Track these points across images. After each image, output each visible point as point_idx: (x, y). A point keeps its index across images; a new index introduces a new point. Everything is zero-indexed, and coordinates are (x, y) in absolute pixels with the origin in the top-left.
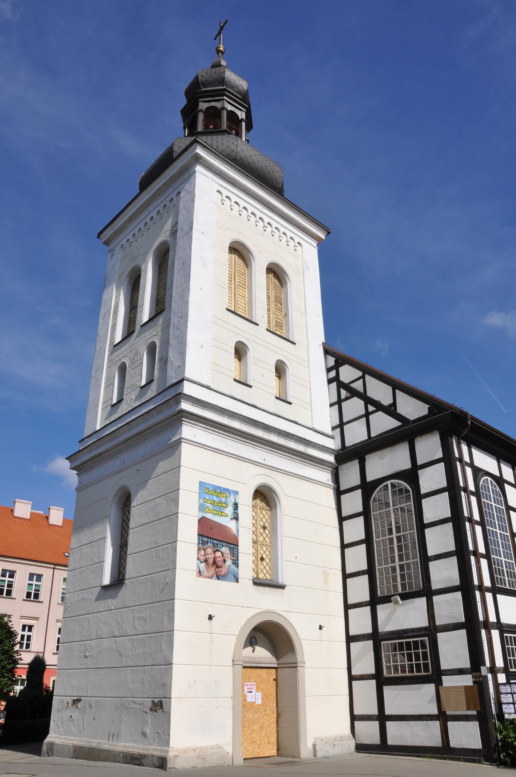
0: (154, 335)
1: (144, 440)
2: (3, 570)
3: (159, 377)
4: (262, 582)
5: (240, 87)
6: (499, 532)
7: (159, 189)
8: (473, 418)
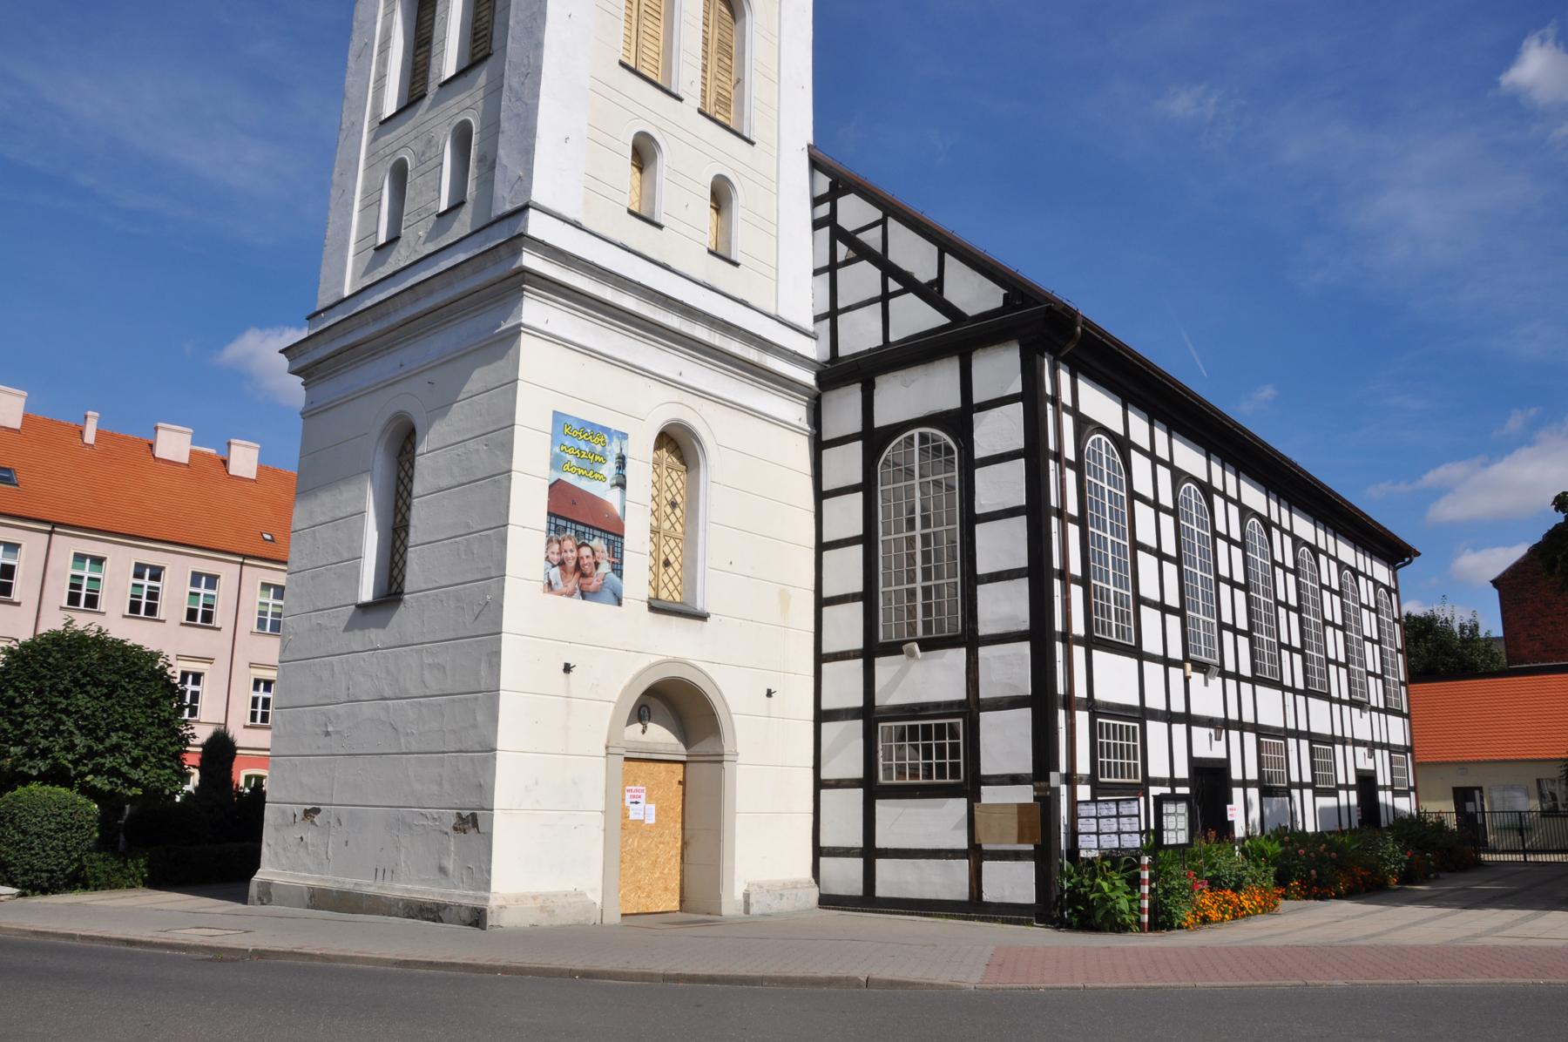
0: (467, 106)
2: (137, 565)
6: (1110, 537)
8: (1086, 322)
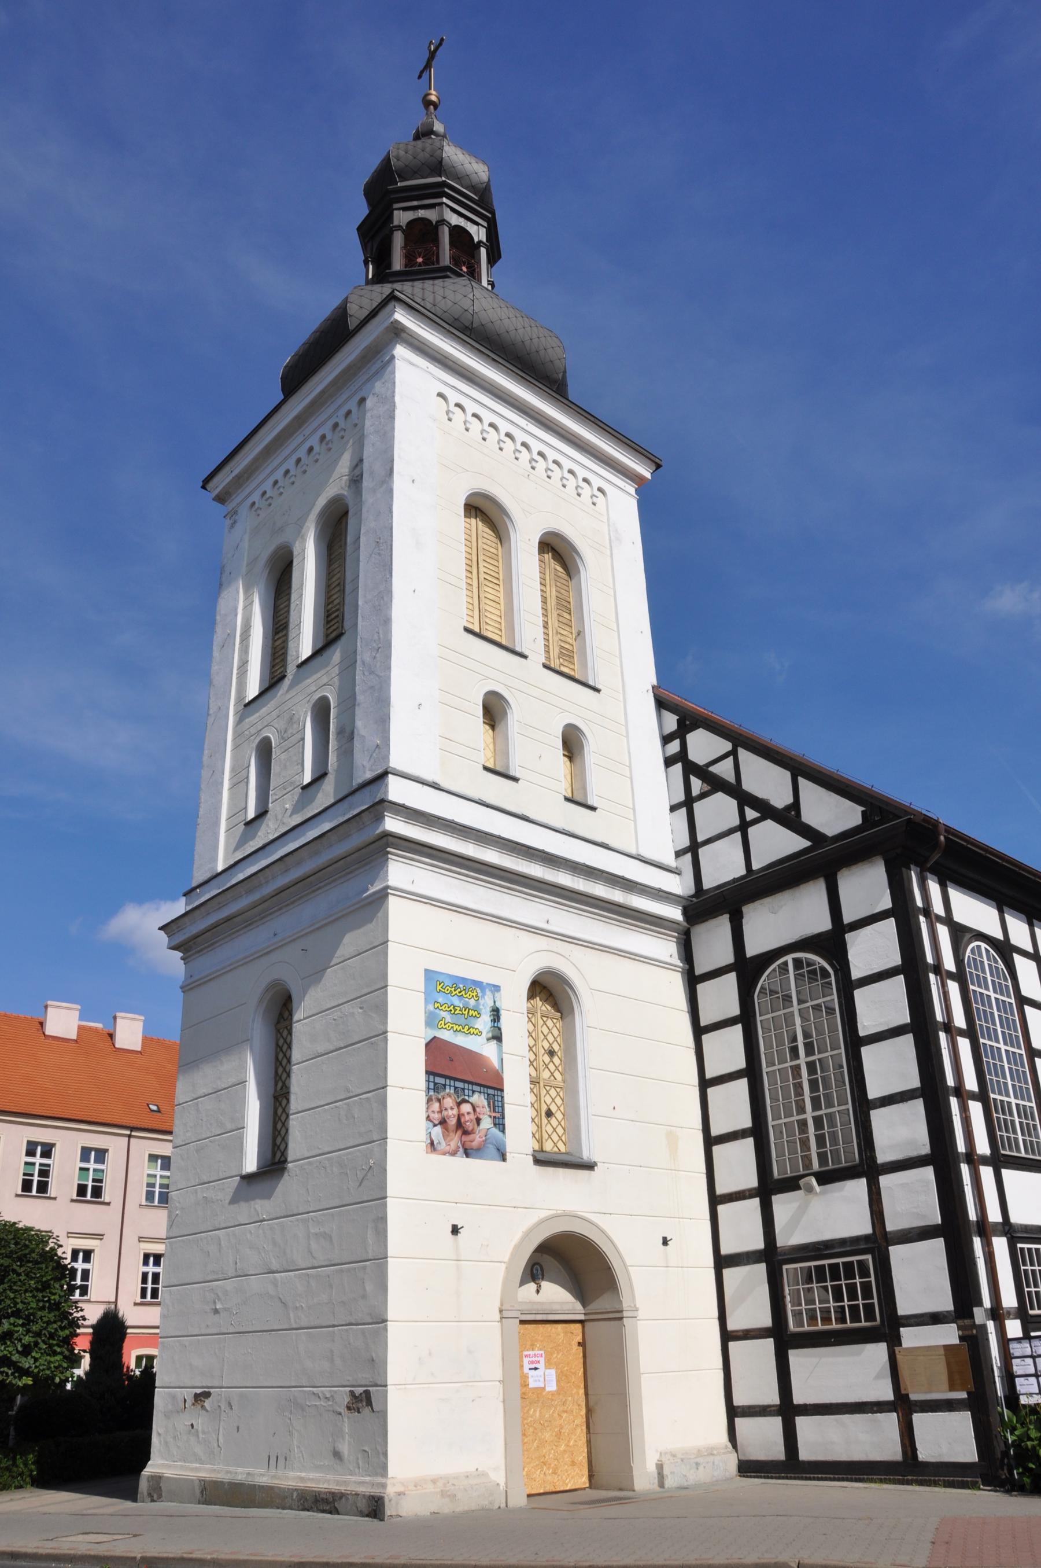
0: (323, 683)
1: (314, 891)
2: (29, 1143)
3: (339, 766)
5: (474, 177)
6: (1003, 1047)
7: (323, 392)
8: (949, 830)
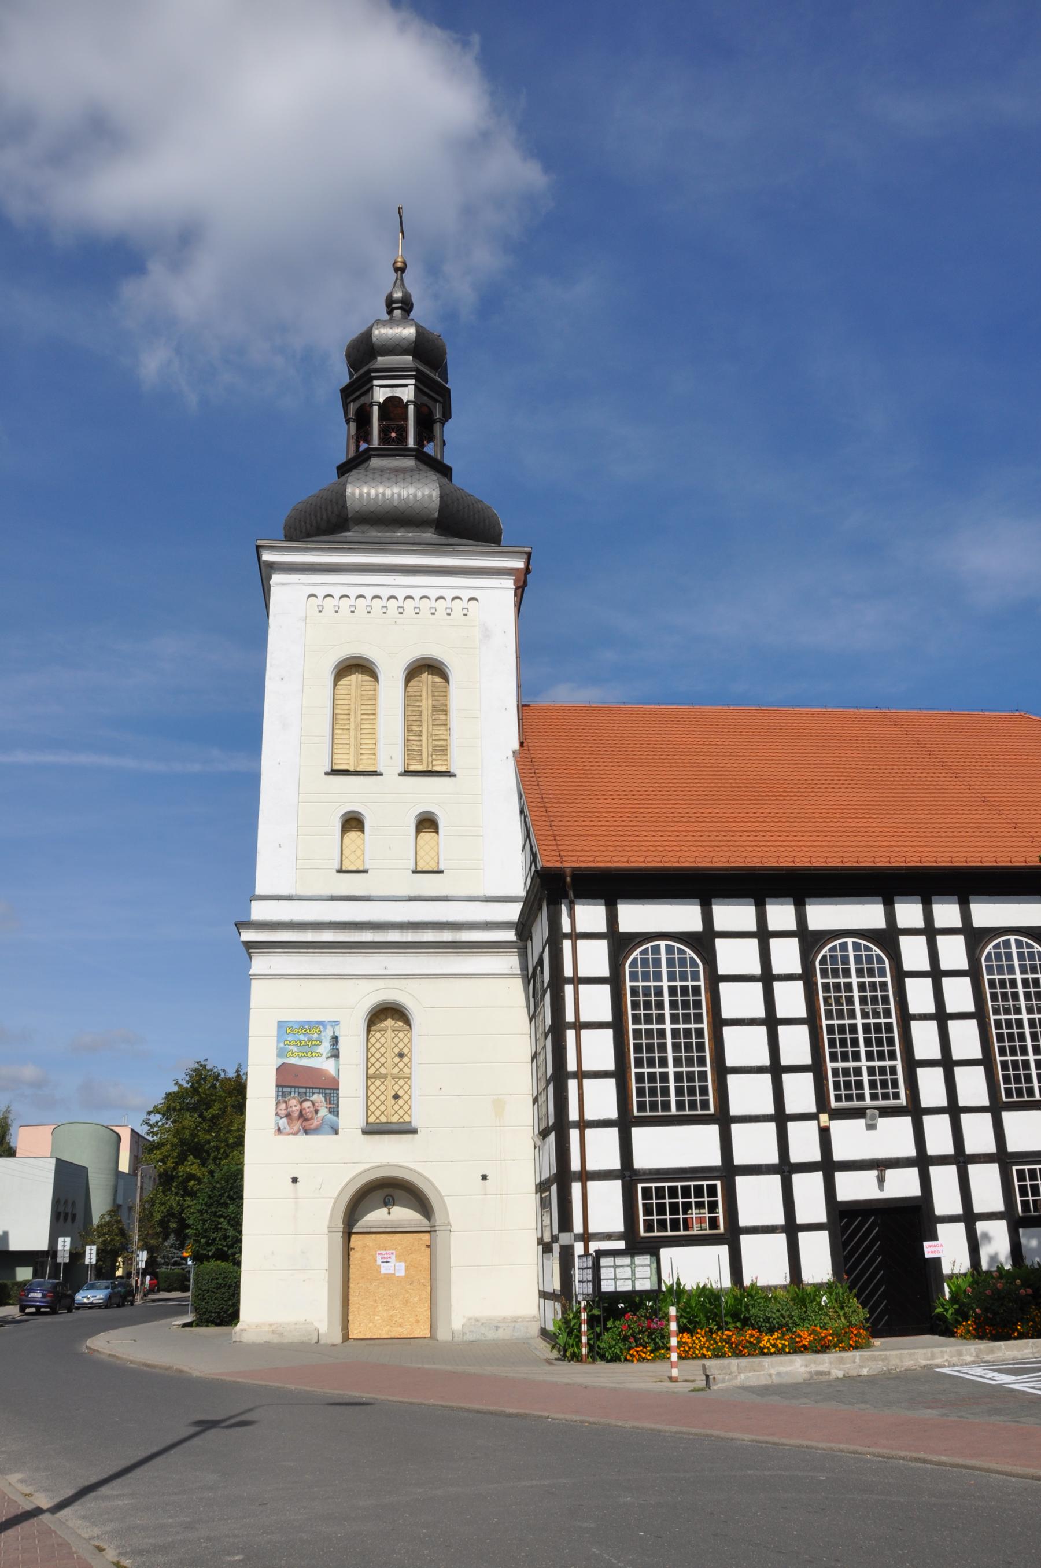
4: (376, 1128)
